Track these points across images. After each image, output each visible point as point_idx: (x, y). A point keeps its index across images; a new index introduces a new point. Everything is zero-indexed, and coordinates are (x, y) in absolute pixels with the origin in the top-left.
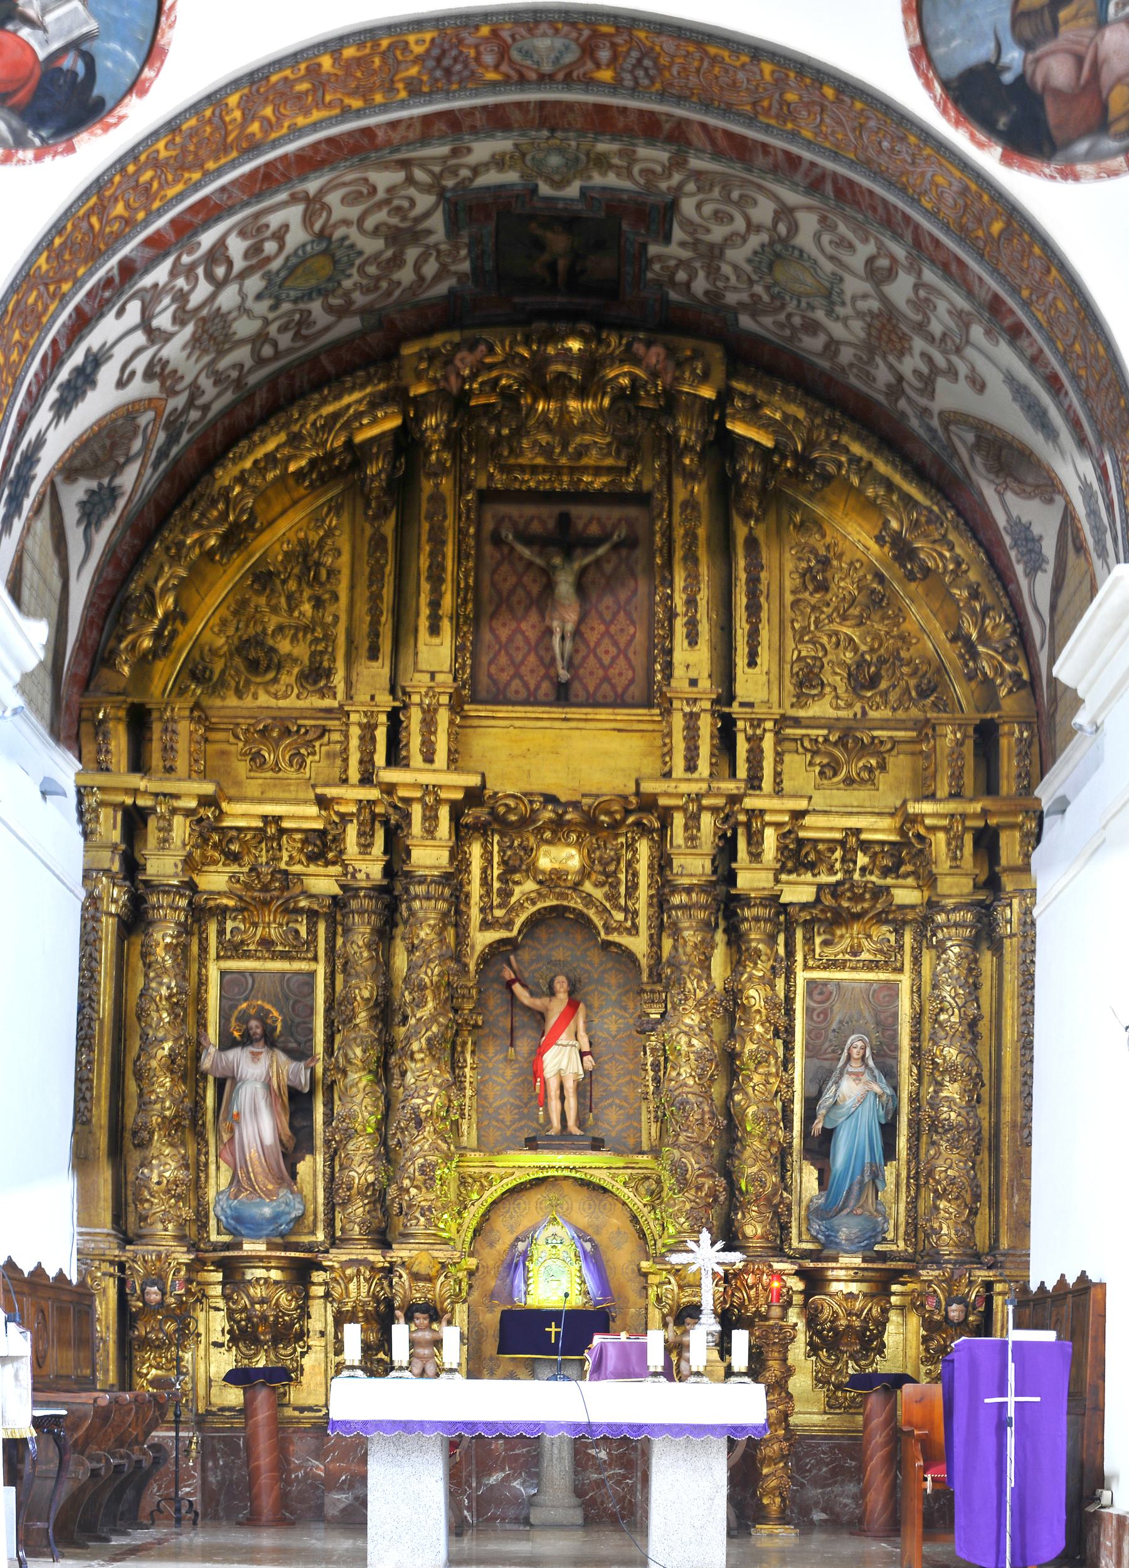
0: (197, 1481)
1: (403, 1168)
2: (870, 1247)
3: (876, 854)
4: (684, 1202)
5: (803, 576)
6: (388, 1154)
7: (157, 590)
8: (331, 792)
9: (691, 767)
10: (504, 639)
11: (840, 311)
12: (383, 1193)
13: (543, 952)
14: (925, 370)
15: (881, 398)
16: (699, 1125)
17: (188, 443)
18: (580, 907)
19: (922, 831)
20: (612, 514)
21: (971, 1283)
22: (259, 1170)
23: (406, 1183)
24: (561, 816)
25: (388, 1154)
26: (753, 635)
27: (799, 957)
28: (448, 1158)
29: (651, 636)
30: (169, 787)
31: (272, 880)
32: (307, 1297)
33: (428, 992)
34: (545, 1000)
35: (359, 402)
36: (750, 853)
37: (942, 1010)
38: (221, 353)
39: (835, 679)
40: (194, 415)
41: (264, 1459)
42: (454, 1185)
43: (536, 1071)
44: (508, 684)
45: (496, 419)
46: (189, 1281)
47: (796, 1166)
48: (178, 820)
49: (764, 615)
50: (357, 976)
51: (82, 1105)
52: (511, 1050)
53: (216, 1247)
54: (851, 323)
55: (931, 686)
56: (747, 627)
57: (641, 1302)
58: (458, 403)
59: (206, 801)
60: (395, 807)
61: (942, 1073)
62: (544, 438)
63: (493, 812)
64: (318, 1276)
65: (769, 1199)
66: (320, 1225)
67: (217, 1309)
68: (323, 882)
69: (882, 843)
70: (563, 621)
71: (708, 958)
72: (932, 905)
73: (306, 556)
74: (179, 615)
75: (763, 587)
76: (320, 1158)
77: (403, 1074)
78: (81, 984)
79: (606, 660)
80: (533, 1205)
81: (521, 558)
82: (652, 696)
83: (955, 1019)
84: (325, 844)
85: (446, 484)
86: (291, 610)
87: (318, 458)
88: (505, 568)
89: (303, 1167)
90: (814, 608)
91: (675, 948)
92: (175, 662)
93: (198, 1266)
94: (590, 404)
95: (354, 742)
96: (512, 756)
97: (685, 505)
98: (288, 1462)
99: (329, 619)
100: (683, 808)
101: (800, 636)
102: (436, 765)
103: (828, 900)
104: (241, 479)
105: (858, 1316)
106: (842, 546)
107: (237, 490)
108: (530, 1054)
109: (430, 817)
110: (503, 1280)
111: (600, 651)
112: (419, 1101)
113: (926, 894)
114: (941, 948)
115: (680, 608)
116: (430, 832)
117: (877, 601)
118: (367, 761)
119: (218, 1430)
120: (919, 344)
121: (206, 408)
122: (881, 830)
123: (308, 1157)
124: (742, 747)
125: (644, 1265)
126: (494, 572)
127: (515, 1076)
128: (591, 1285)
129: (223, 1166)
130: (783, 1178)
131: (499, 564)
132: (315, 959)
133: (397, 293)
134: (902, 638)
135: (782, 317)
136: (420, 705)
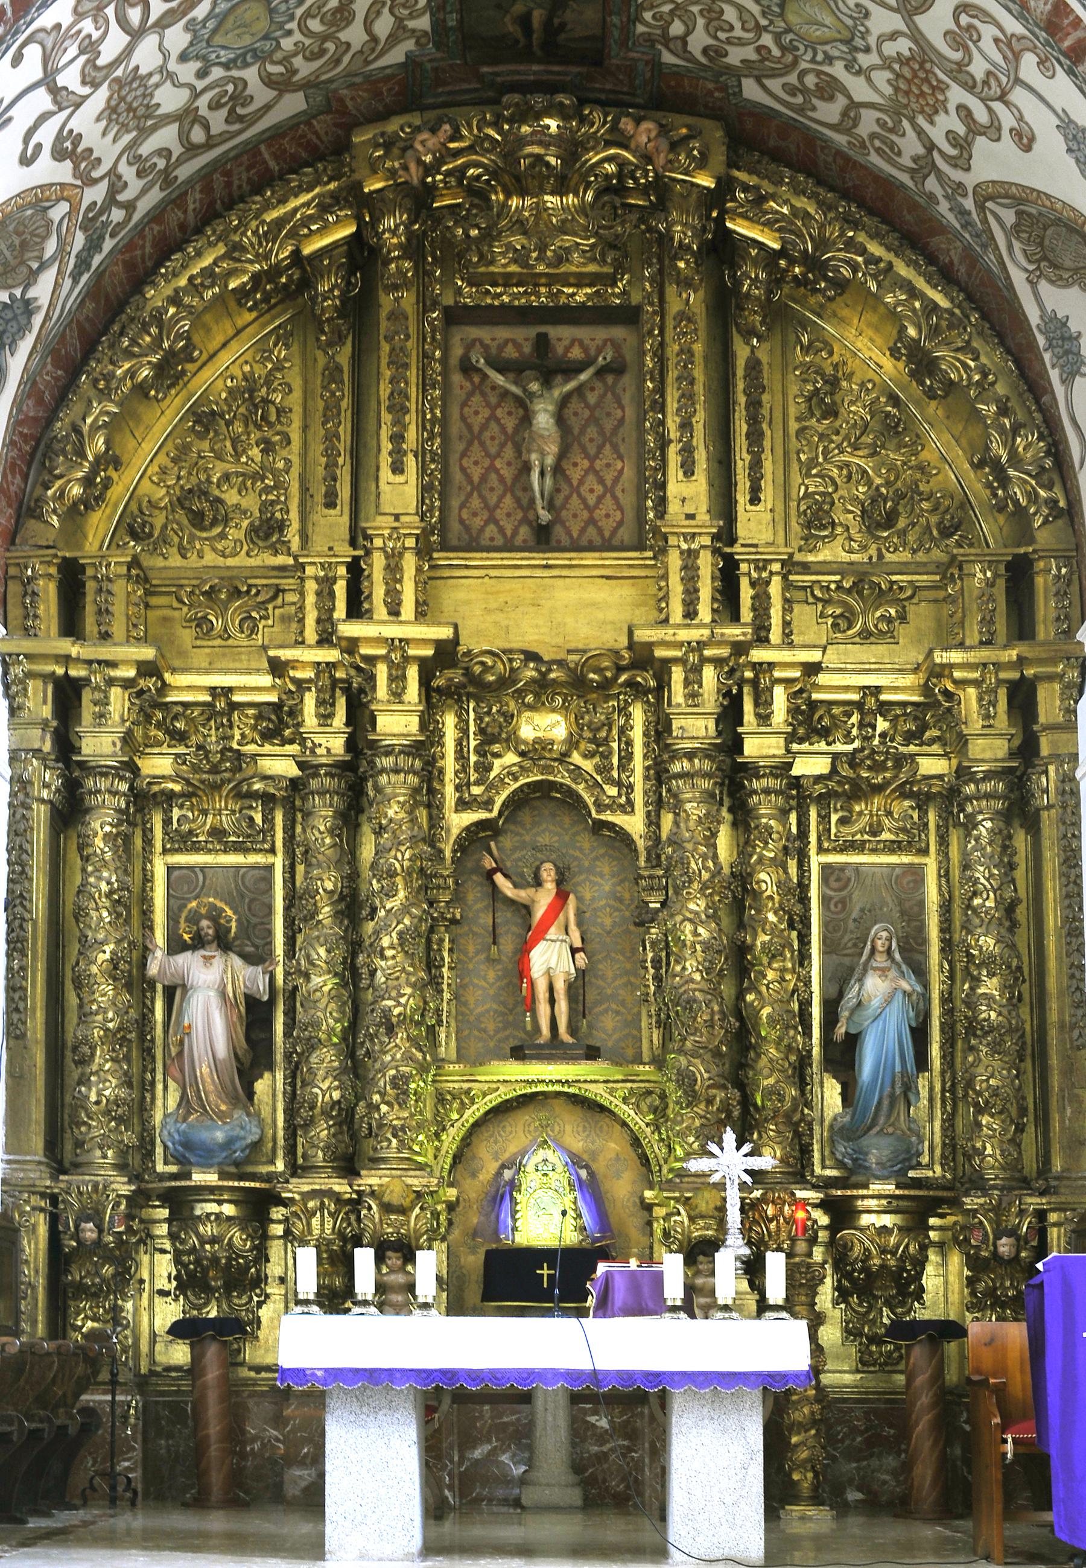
0: (137, 1454)
1: (373, 1081)
2: (903, 1172)
3: (897, 717)
4: (692, 1118)
5: (809, 400)
6: (355, 1068)
7: (86, 429)
8: (285, 654)
9: (690, 613)
10: (476, 479)
11: (865, 60)
12: (351, 1111)
13: (527, 838)
14: (961, 130)
15: (905, 178)
16: (707, 1026)
17: (111, 252)
18: (568, 781)
19: (950, 687)
20: (594, 335)
21: (1021, 1213)
22: (211, 1088)
23: (376, 1098)
24: (544, 675)
25: (355, 1068)
26: (756, 465)
27: (813, 838)
28: (423, 1069)
29: (641, 469)
30: (105, 652)
31: (222, 760)
32: (265, 1237)
33: (399, 880)
34: (531, 891)
35: (307, 205)
36: (758, 715)
37: (975, 894)
38: (144, 133)
39: (847, 516)
40: (117, 215)
41: (214, 1429)
42: (430, 1103)
43: (522, 969)
44: (482, 530)
45: (466, 222)
46: (129, 1217)
47: (816, 1079)
48: (115, 692)
49: (767, 444)
50: (319, 866)
51: (15, 1017)
52: (494, 949)
53: (162, 1177)
54: (875, 75)
55: (955, 522)
56: (747, 458)
57: (645, 1241)
58: (419, 200)
59: (147, 669)
60: (358, 669)
61: (979, 967)
62: (517, 241)
63: (467, 672)
64: (278, 1213)
65: (788, 1116)
66: (280, 1153)
67: (163, 1251)
68: (279, 764)
69: (904, 704)
70: (543, 454)
71: (714, 835)
72: (963, 773)
73: (252, 391)
74: (111, 460)
75: (765, 411)
76: (280, 1076)
77: (373, 973)
78: (10, 881)
79: (592, 500)
80: (520, 1128)
81: (494, 388)
82: (646, 537)
83: (990, 904)
84: (281, 720)
85: (408, 299)
86: (237, 455)
87: (262, 272)
88: (477, 399)
89: (261, 1086)
90: (822, 437)
91: (676, 823)
92: (110, 517)
93: (141, 1200)
94: (571, 199)
95: (311, 599)
96: (488, 611)
97: (682, 316)
98: (243, 1432)
99: (281, 465)
100: (682, 661)
101: (807, 469)
102: (403, 618)
103: (845, 771)
104: (175, 300)
105: (893, 1253)
106: (852, 365)
107: (172, 310)
108: (515, 953)
109: (397, 679)
110: (487, 1215)
111: (584, 490)
112: (391, 1003)
113: (955, 762)
114: (970, 825)
115: (674, 434)
116: (397, 695)
117: (892, 428)
118: (326, 623)
119: (163, 1394)
120: (956, 95)
121: (129, 207)
122: (901, 687)
123: (267, 1075)
124: (746, 593)
125: (648, 1194)
126: (464, 404)
127: (499, 978)
128: (587, 1219)
129: (172, 1085)
130: (803, 1092)
131: (470, 394)
132: (273, 851)
133: (346, 59)
134: (921, 468)
135: (792, 79)
136: (383, 549)
